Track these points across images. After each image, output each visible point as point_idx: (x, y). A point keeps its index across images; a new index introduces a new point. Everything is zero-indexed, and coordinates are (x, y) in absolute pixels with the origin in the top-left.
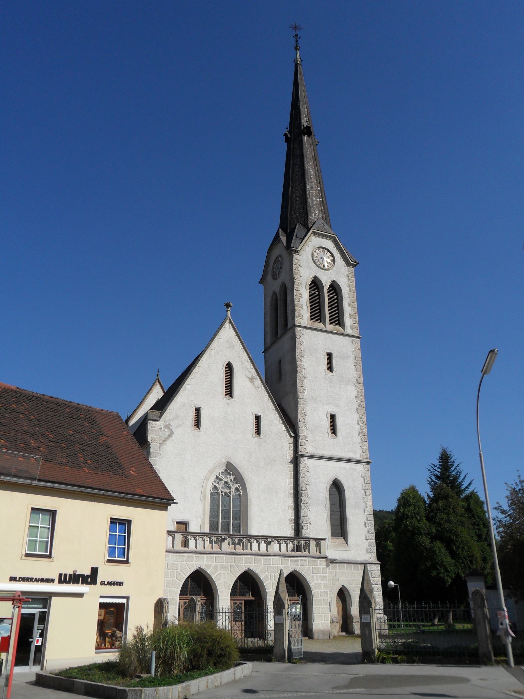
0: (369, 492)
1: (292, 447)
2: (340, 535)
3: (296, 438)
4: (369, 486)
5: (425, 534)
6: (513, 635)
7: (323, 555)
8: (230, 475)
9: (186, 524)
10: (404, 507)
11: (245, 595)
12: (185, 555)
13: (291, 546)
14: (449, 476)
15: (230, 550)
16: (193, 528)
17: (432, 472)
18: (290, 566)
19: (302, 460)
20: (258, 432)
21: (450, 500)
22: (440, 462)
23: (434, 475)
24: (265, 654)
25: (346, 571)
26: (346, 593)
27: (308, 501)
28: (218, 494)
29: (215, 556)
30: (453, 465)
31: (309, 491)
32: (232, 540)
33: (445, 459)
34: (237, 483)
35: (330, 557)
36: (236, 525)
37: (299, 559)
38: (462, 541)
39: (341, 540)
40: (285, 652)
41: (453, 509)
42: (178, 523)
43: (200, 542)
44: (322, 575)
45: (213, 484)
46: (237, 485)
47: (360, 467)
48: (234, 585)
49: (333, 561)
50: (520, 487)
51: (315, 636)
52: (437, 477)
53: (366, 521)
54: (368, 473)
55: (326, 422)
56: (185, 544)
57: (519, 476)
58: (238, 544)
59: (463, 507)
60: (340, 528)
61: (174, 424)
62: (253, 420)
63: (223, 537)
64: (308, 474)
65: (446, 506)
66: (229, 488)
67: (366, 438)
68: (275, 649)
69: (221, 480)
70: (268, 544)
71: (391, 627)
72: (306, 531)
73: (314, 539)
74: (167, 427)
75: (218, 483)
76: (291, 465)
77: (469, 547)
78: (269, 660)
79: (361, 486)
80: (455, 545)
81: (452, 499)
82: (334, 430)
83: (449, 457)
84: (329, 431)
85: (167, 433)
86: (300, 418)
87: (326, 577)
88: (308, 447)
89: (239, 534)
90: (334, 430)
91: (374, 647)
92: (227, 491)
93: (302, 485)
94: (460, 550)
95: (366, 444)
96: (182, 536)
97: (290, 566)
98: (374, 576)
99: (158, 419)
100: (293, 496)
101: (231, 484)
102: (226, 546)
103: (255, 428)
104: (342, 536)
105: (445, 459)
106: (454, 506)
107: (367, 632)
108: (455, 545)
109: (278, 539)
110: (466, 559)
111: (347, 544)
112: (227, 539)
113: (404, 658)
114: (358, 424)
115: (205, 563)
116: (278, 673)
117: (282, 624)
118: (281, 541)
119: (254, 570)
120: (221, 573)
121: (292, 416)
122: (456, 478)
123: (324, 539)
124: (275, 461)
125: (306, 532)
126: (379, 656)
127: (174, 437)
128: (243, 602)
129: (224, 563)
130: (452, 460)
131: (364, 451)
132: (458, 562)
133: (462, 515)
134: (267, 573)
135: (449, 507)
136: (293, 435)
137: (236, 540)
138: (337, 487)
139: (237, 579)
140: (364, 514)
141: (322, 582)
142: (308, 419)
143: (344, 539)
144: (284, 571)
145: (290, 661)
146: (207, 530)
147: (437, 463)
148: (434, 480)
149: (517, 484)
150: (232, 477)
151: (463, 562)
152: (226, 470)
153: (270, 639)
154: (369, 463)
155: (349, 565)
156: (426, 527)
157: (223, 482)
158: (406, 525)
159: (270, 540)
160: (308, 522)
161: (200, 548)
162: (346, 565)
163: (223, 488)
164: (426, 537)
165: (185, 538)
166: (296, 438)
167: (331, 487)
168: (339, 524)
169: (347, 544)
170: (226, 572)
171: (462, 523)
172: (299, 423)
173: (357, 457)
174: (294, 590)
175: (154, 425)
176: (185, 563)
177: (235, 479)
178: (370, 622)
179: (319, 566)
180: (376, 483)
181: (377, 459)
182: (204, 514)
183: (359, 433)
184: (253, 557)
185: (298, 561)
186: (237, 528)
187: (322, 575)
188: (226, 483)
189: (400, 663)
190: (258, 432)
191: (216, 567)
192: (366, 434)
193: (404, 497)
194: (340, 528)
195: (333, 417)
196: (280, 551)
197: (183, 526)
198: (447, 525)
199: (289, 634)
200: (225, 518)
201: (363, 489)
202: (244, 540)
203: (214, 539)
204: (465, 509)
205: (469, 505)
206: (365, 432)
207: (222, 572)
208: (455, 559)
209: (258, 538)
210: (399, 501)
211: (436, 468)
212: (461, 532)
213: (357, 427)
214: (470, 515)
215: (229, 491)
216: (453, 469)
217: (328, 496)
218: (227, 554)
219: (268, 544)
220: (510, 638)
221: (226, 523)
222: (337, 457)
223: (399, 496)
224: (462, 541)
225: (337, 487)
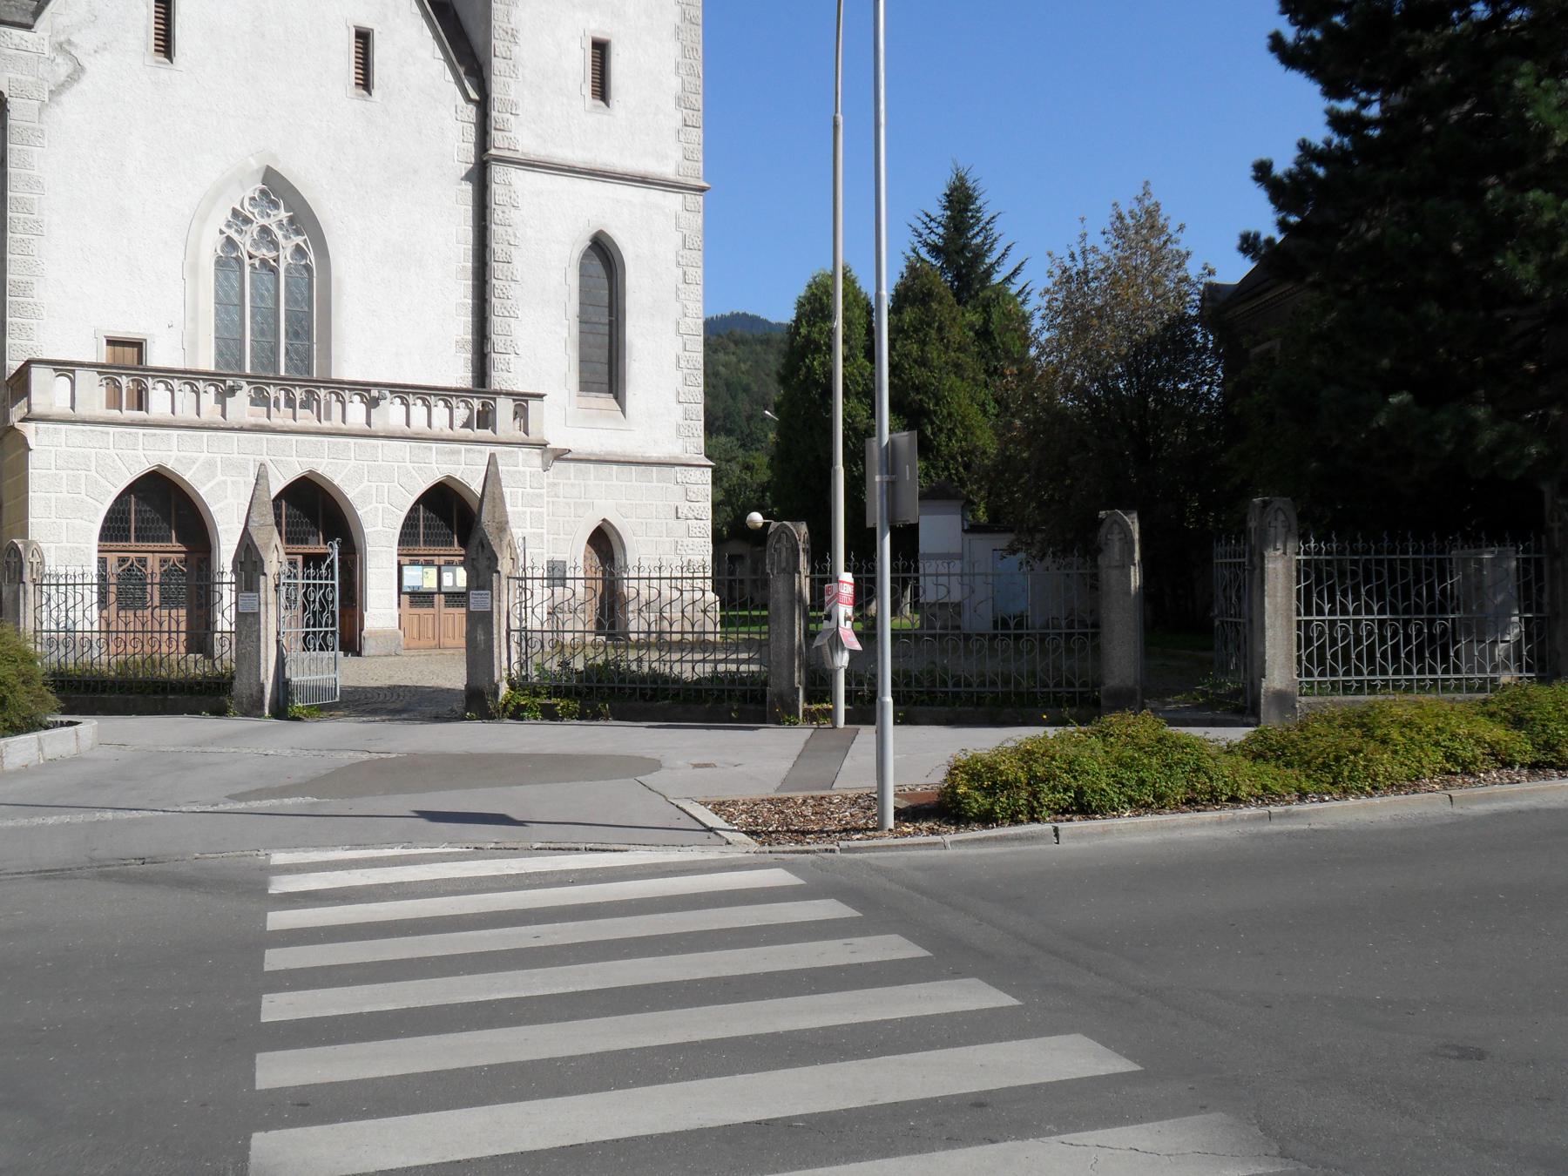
0: (697, 274)
1: (471, 133)
2: (606, 387)
3: (483, 106)
4: (697, 257)
5: (858, 393)
6: (858, 647)
7: (533, 437)
8: (276, 206)
9: (138, 345)
10: (811, 324)
11: (305, 541)
12: (111, 430)
13: (461, 413)
14: (965, 247)
15: (253, 420)
16: (155, 358)
17: (920, 235)
18: (434, 465)
19: (498, 173)
20: (365, 81)
21: (934, 305)
22: (946, 208)
23: (926, 244)
24: (209, 695)
25: (615, 482)
26: (613, 539)
27: (514, 291)
28: (239, 261)
29: (206, 434)
30: (979, 220)
31: (518, 265)
32: (287, 392)
33: (960, 201)
34: (298, 233)
35: (556, 443)
36: (297, 352)
37: (463, 447)
38: (950, 415)
39: (606, 401)
40: (262, 692)
41: (940, 329)
42: (112, 342)
43: (185, 397)
44: (529, 490)
45: (222, 232)
46: (299, 240)
47: (674, 200)
48: (408, 518)
49: (560, 456)
50: (1080, 266)
51: (369, 647)
52: (934, 250)
53: (680, 352)
54: (699, 220)
55: (580, 62)
56: (140, 402)
57: (1084, 236)
58: (305, 405)
59: (972, 327)
60: (604, 368)
61: (84, 42)
62: (349, 44)
63: (229, 383)
64: (514, 215)
65: (922, 321)
66: (275, 245)
67: (697, 118)
68: (236, 683)
69: (247, 221)
70: (372, 403)
71: (725, 622)
72: (505, 375)
73: (508, 394)
74: (62, 48)
75: (240, 232)
76: (468, 188)
77: (968, 430)
78: (220, 711)
79: (672, 256)
80: (932, 423)
81: (940, 303)
82: (602, 89)
83: (970, 197)
84: (588, 89)
85: (63, 68)
86: (499, 44)
87: (540, 496)
88: (518, 132)
89: (305, 377)
90: (602, 89)
91: (496, 678)
92: (269, 255)
93: (497, 247)
94: (943, 437)
95: (697, 135)
96: (98, 377)
97: (434, 465)
98: (692, 496)
99: (29, 20)
100: (470, 275)
101: (279, 234)
102: (241, 407)
103: (353, 70)
104: (610, 391)
105: (960, 201)
106: (941, 323)
107: (481, 637)
108: (932, 423)
109: (425, 393)
110: (953, 458)
111: (623, 412)
112: (241, 388)
113: (575, 706)
114: (677, 73)
115: (175, 453)
116: (185, 749)
117: (257, 615)
118: (411, 399)
119: (328, 475)
120: (225, 482)
121: (476, 38)
122: (979, 255)
123: (540, 396)
124: (416, 172)
125: (498, 380)
126: (508, 702)
127: (85, 84)
128: (300, 558)
129: (236, 455)
130: (979, 203)
131: (689, 155)
132: (934, 467)
133: (961, 348)
134: (366, 483)
135: (929, 325)
136: (474, 95)
137: (299, 394)
138: (602, 254)
139: (418, 502)
140: (678, 332)
141: (528, 510)
142: (522, 51)
143: (616, 398)
144: (272, 471)
145: (281, 710)
146: (206, 361)
147: (938, 212)
148: (928, 258)
149: (1072, 256)
150: (283, 215)
151: (946, 468)
152: (263, 192)
153: (225, 651)
154: (702, 190)
155: (626, 468)
156: (862, 375)
157: (255, 228)
158: (810, 369)
159: (375, 393)
160: (510, 350)
161: (186, 410)
162: (615, 467)
163: (255, 243)
164: (860, 401)
165: (139, 383)
166: (483, 106)
167: (585, 256)
168: (605, 359)
169: (623, 412)
170: (241, 480)
171: (958, 368)
172: (494, 60)
173: (668, 171)
174: (451, 528)
175: (17, 41)
176: (112, 452)
177: (291, 220)
178: (258, 614)
179: (521, 468)
180: (719, 247)
181: (726, 183)
182: (194, 319)
183: (680, 101)
184: (326, 439)
185: (459, 452)
186: (302, 359)
187: (529, 490)
188: (265, 230)
189: (562, 719)
190: (365, 81)
191: (210, 464)
192: (699, 104)
193: (813, 294)
194: (604, 368)
195: (601, 49)
196: (430, 425)
197: (131, 353)
198: (916, 371)
199: (278, 642)
200: (296, 335)
201: (678, 264)
202: (322, 393)
203: (299, 394)
204: (976, 333)
205: (987, 322)
206: (698, 101)
207: (229, 479)
208: (926, 459)
209: (361, 388)
210: (800, 305)
211: (933, 224)
212: (951, 389)
213: (674, 84)
214: (986, 347)
215: (274, 254)
216: (977, 229)
217: (574, 281)
218: (241, 429)
219: (372, 403)
220: (846, 656)
221: (267, 346)
222: (608, 168)
223: (802, 291)
224: (950, 415)
225: (602, 254)
